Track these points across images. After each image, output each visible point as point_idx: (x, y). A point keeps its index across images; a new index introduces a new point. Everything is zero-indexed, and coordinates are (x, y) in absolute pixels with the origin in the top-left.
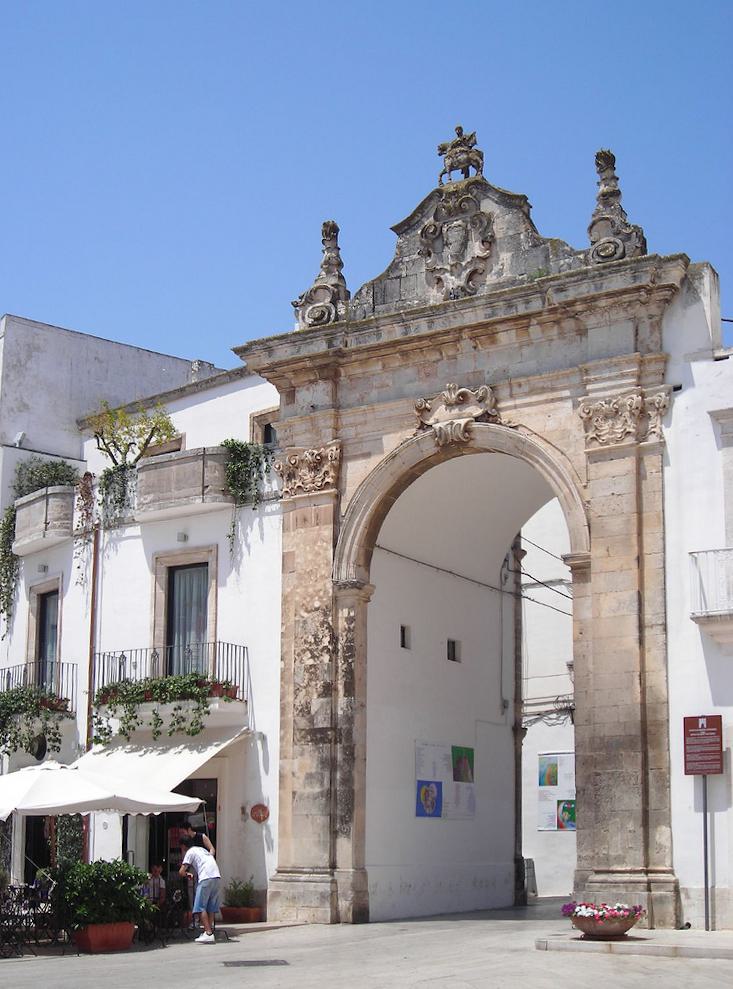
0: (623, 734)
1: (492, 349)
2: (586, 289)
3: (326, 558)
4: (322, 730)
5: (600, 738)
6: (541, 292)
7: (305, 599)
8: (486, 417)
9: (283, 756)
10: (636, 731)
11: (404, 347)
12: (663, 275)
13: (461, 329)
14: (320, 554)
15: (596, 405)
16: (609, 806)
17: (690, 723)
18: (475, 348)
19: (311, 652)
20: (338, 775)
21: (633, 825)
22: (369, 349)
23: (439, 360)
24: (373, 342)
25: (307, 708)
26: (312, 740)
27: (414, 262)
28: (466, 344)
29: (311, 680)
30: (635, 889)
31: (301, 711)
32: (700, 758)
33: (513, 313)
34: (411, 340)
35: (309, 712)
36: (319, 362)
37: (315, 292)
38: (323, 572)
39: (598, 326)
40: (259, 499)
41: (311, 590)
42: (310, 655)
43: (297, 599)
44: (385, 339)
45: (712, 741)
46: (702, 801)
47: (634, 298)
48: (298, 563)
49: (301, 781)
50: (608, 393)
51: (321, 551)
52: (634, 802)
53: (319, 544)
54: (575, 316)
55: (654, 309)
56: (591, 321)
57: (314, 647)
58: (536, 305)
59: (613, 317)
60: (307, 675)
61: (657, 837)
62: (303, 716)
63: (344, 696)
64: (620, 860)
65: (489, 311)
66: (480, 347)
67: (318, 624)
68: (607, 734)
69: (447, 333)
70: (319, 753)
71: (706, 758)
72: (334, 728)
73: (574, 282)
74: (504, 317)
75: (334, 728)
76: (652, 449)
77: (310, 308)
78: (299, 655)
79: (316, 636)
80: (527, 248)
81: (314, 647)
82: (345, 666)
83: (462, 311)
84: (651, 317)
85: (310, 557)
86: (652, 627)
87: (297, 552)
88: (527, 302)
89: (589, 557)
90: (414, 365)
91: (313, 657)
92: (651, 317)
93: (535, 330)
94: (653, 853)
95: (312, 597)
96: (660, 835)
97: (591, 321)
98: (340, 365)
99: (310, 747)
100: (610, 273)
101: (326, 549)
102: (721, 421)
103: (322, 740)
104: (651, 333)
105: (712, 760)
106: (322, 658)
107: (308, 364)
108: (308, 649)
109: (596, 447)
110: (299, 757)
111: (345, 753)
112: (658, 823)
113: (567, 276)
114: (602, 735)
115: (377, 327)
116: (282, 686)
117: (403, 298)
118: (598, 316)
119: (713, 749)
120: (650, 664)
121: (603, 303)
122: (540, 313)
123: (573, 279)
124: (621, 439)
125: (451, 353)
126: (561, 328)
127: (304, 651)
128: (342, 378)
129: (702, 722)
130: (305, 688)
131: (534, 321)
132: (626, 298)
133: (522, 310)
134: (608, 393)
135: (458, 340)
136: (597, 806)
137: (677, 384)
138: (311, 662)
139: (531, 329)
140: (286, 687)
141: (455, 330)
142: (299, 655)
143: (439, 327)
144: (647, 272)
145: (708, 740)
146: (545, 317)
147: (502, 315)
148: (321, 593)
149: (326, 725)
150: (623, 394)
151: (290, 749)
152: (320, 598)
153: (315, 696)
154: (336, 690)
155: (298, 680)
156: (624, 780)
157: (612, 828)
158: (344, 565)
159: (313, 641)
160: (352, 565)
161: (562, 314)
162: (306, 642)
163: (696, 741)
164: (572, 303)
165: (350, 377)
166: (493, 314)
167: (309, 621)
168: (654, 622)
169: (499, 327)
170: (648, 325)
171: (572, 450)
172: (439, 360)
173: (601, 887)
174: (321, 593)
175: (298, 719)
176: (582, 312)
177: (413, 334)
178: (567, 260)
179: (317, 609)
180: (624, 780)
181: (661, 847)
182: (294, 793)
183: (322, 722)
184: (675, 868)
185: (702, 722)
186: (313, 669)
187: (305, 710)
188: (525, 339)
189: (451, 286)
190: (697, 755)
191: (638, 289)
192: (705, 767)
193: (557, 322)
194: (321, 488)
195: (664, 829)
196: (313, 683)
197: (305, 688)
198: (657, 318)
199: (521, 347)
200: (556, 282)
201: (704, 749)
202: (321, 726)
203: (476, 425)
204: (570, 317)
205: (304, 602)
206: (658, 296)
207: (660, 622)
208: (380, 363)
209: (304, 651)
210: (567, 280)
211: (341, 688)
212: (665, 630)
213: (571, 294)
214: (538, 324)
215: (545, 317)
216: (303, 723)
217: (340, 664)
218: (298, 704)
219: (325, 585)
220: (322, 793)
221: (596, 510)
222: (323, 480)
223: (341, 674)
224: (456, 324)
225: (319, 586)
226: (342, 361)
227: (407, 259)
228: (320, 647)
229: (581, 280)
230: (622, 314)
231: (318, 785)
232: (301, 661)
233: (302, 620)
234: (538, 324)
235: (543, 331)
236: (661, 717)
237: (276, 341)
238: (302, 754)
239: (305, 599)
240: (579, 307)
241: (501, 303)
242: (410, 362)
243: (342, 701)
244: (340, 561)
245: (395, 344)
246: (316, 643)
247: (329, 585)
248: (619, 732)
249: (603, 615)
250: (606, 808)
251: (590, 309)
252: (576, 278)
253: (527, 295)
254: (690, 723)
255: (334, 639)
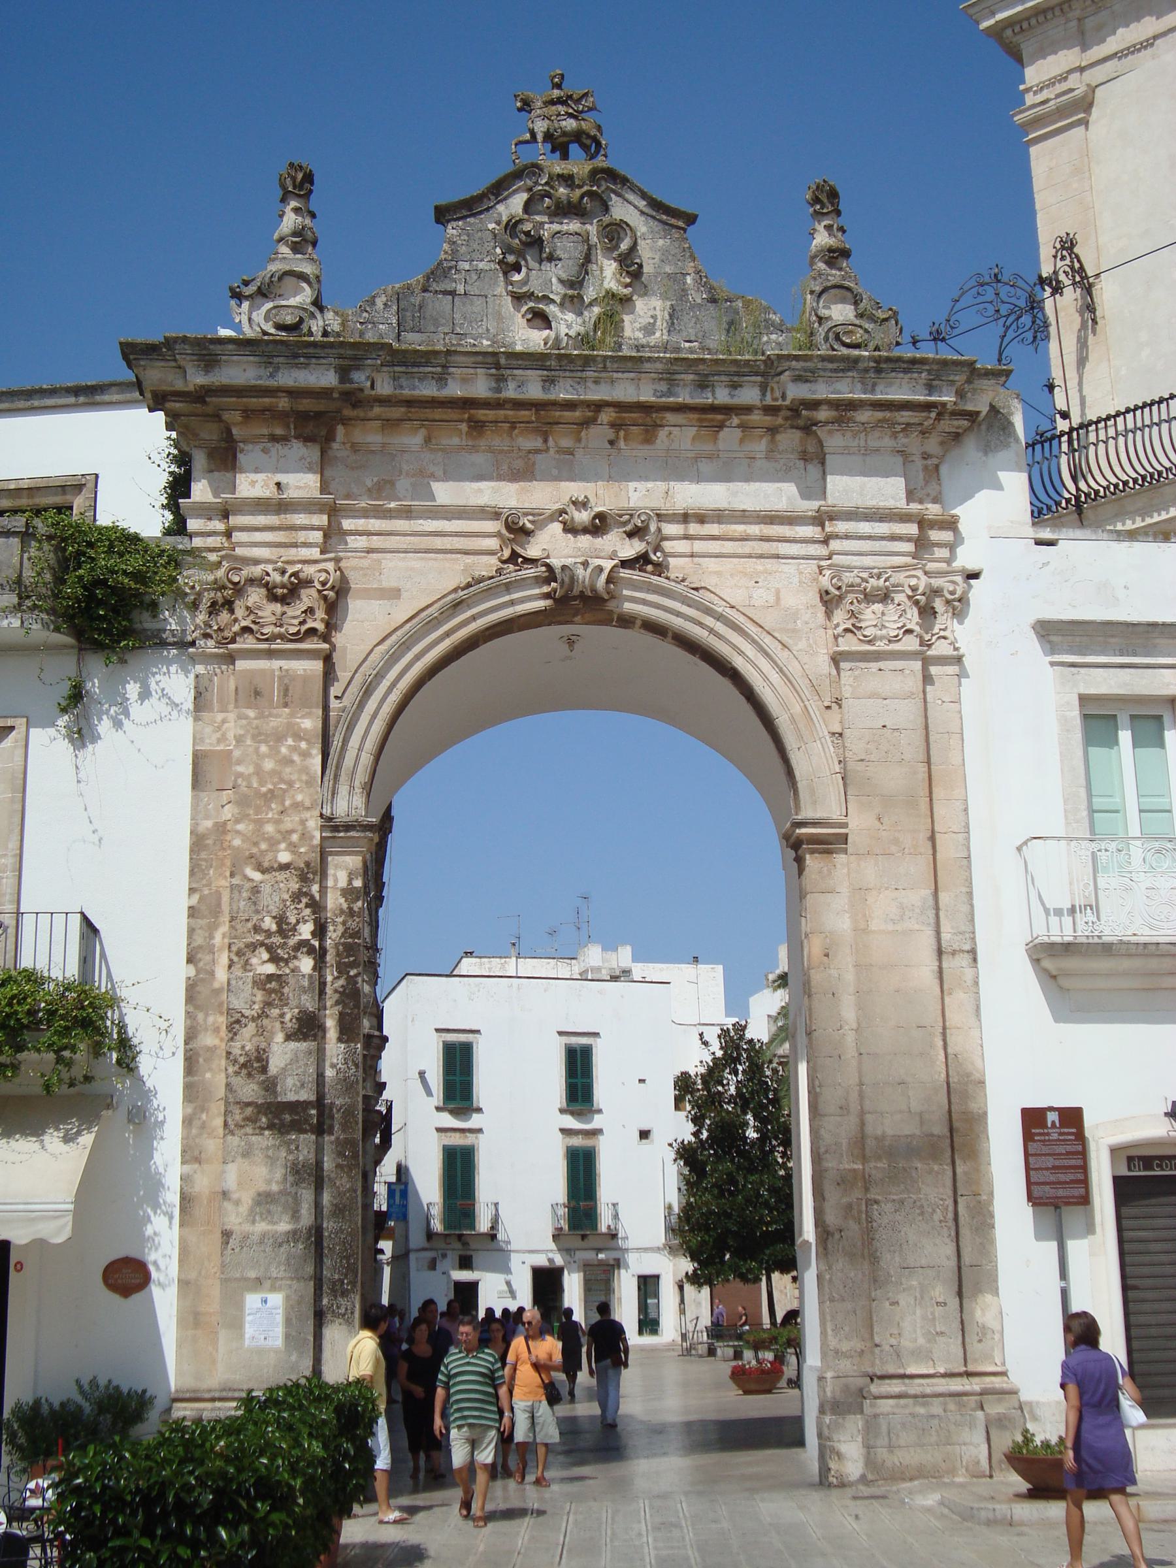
0: (918, 1132)
1: (643, 451)
2: (847, 389)
3: (305, 770)
4: (294, 1106)
5: (876, 1138)
6: (763, 374)
7: (256, 844)
8: (642, 560)
9: (191, 1154)
10: (940, 1129)
11: (481, 414)
12: (969, 394)
13: (599, 406)
14: (292, 762)
15: (849, 578)
16: (897, 1259)
17: (1032, 1119)
18: (611, 443)
19: (269, 949)
20: (326, 1198)
21: (942, 1291)
22: (409, 403)
23: (537, 451)
24: (428, 390)
25: (259, 1059)
26: (270, 1127)
27: (479, 272)
28: (599, 434)
29: (268, 1004)
30: (962, 1406)
31: (244, 1066)
32: (1052, 1178)
33: (707, 398)
34: (499, 404)
35: (264, 1069)
36: (306, 404)
37: (280, 279)
38: (299, 798)
39: (846, 451)
40: (158, 641)
41: (269, 828)
42: (266, 956)
43: (237, 842)
44: (455, 390)
45: (1069, 1148)
46: (188, 1395)
47: (916, 420)
48: (240, 775)
49: (244, 1209)
50: (868, 561)
51: (296, 758)
52: (941, 1251)
53: (290, 742)
54: (808, 428)
55: (932, 445)
56: (834, 441)
57: (277, 940)
58: (749, 395)
59: (873, 443)
60: (260, 996)
61: (978, 1314)
62: (249, 1075)
63: (340, 1040)
64: (921, 1354)
65: (663, 387)
66: (622, 444)
67: (286, 896)
68: (890, 1132)
69: (570, 405)
70: (290, 1152)
71: (1062, 1177)
72: (320, 1103)
73: (831, 371)
74: (689, 400)
75: (320, 1103)
76: (943, 660)
77: (270, 305)
78: (239, 953)
79: (281, 920)
80: (699, 301)
81: (277, 940)
82: (341, 982)
83: (615, 375)
84: (926, 456)
85: (269, 765)
86: (954, 953)
87: (237, 754)
88: (735, 386)
89: (845, 825)
90: (490, 450)
91: (274, 959)
92: (926, 456)
93: (730, 436)
94: (974, 1347)
95: (273, 843)
96: (983, 1311)
97: (834, 441)
98: (345, 422)
99: (267, 1139)
100: (893, 370)
101: (305, 755)
102: (1054, 638)
103: (297, 1127)
104: (927, 482)
105: (1072, 1182)
106: (296, 963)
107: (283, 403)
108: (262, 944)
109: (849, 644)
110: (239, 1160)
111: (341, 1154)
112: (978, 1290)
113: (823, 359)
114: (879, 1132)
115: (444, 366)
116: (187, 1013)
117: (458, 330)
118: (848, 434)
119: (1073, 1162)
120: (953, 1018)
121: (864, 416)
122: (747, 409)
123: (830, 366)
124: (895, 639)
125: (566, 443)
126: (773, 441)
127: (253, 947)
128: (335, 446)
129: (1052, 1117)
130: (253, 1019)
131: (735, 421)
132: (906, 416)
133: (722, 396)
134: (868, 561)
135: (586, 423)
136: (874, 1259)
137: (972, 566)
138: (270, 969)
139: (724, 434)
140: (200, 1016)
141: (588, 404)
142: (239, 953)
143: (563, 392)
144: (952, 382)
145: (1061, 1149)
146: (756, 417)
147: (684, 397)
148: (295, 837)
149: (307, 1095)
150: (897, 568)
151: (211, 1145)
152: (293, 847)
153: (280, 1037)
154: (322, 1028)
155: (237, 1004)
156: (922, 1214)
157: (904, 1299)
158: (343, 789)
159: (274, 927)
160: (358, 790)
161: (786, 419)
162: (257, 929)
163: (1045, 1150)
164: (815, 405)
165: (355, 448)
166: (670, 393)
167: (266, 889)
168: (956, 947)
169: (670, 417)
170: (920, 468)
171: (802, 645)
172: (537, 451)
173: (897, 1406)
174: (295, 837)
175: (237, 1081)
176: (827, 423)
177: (510, 392)
178: (773, 337)
179: (285, 867)
180: (922, 1214)
181: (984, 1330)
182: (227, 1235)
183: (295, 1090)
184: (1009, 1366)
185: (1052, 1117)
186: (274, 985)
187: (256, 1064)
188: (708, 447)
189: (563, 330)
190: (1046, 1173)
191: (928, 406)
192: (1061, 1193)
193: (773, 431)
194: (298, 637)
195: (989, 1298)
196: (275, 1012)
197: (253, 1019)
198: (935, 461)
199: (696, 459)
200: (801, 364)
201: (1057, 1163)
202: (291, 1097)
203: (625, 573)
204: (797, 428)
205: (255, 850)
206: (948, 425)
207: (967, 947)
208: (422, 433)
209: (253, 947)
210: (820, 365)
211: (331, 1024)
212: (975, 960)
213: (821, 391)
214: (738, 426)
215: (756, 417)
216: (250, 1090)
217: (329, 978)
218: (236, 1051)
219: (303, 822)
220: (294, 1235)
221: (856, 745)
222: (302, 623)
223: (331, 997)
224: (595, 394)
225: (290, 822)
226: (348, 412)
227: (467, 266)
228: (292, 942)
229: (843, 370)
230: (887, 442)
231: (286, 1218)
232: (246, 966)
233: (248, 885)
234: (738, 426)
235: (742, 441)
236: (973, 1106)
237: (231, 347)
238: (246, 1154)
239: (256, 844)
240: (823, 414)
241: (691, 377)
242: (482, 443)
243: (335, 1049)
244: (336, 777)
245: (468, 403)
246: (281, 932)
247: (314, 824)
248: (910, 1128)
249: (873, 926)
250: (890, 1261)
251: (839, 421)
252: (834, 366)
253: (738, 374)
254: (1032, 1119)
255: (320, 930)
